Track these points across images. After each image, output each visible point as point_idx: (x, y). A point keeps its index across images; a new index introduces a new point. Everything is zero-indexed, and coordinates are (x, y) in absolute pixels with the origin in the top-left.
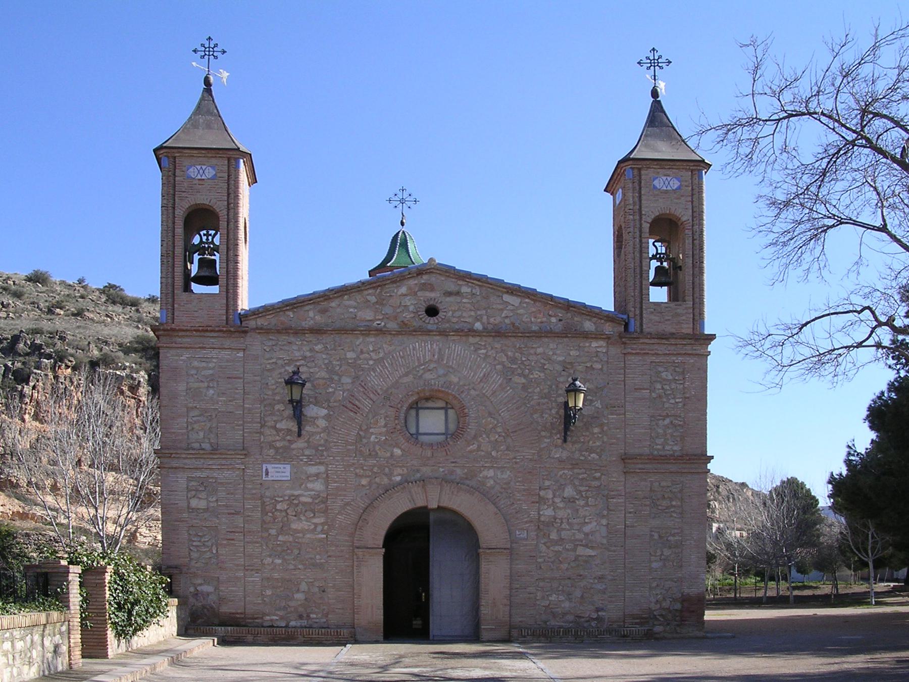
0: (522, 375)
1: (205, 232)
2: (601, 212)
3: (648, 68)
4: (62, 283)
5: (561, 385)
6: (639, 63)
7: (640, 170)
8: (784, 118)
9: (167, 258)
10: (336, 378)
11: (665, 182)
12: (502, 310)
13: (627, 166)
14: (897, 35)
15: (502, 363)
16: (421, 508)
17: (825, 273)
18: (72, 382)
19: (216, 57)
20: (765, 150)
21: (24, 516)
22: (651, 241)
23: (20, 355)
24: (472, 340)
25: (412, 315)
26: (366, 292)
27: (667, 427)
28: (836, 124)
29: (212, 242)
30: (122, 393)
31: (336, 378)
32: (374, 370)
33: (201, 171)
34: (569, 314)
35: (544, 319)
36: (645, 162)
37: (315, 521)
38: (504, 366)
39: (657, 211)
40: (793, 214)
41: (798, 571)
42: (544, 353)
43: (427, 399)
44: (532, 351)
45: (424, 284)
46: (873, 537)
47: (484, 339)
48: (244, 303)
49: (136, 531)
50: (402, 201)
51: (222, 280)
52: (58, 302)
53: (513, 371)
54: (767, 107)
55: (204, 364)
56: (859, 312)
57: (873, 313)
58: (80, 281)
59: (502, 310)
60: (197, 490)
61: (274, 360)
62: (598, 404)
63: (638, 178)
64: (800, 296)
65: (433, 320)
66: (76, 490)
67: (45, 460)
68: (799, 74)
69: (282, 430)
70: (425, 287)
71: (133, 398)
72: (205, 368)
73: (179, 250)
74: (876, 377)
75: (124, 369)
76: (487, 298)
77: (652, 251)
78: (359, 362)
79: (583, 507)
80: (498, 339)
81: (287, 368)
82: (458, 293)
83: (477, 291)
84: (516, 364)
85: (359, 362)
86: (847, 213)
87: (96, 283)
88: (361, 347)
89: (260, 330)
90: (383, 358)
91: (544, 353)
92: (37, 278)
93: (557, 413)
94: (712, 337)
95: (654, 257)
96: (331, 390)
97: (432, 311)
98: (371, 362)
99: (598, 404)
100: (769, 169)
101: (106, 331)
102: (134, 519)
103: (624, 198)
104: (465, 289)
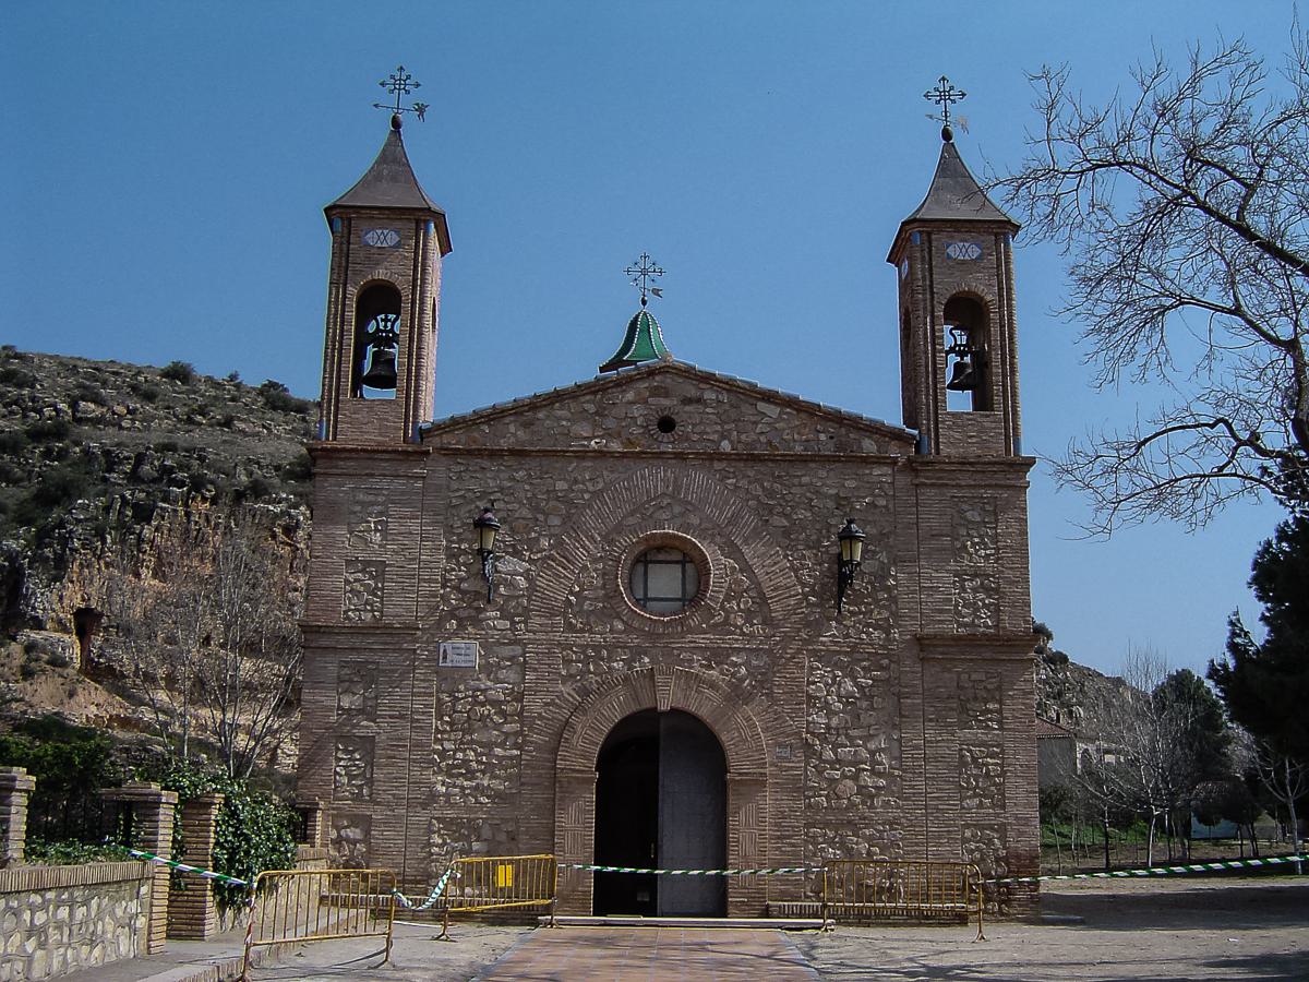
1: (383, 316)
4: (209, 379)
5: (833, 530)
7: (929, 234)
8: (1089, 169)
9: (334, 346)
11: (962, 250)
12: (756, 423)
14: (1221, 61)
15: (757, 498)
16: (647, 710)
17: (1167, 370)
18: (208, 521)
19: (408, 92)
20: (1069, 210)
21: (125, 723)
22: (947, 328)
23: (143, 482)
24: (717, 465)
25: (641, 431)
26: (582, 399)
27: (975, 590)
28: (1154, 178)
29: (392, 330)
30: (274, 536)
32: (590, 507)
34: (843, 429)
36: (932, 225)
39: (952, 285)
40: (1109, 293)
41: (1200, 821)
42: (811, 484)
43: (659, 549)
44: (796, 481)
45: (656, 388)
46: (1291, 765)
48: (428, 414)
50: (644, 272)
51: (402, 382)
52: (200, 406)
53: (771, 509)
54: (1066, 155)
55: (371, 498)
56: (1212, 426)
57: (1229, 426)
58: (233, 377)
59: (756, 423)
63: (927, 244)
64: (1134, 404)
65: (666, 437)
66: (200, 683)
67: (161, 636)
70: (656, 392)
71: (288, 544)
73: (351, 339)
74: (1263, 517)
75: (279, 502)
77: (948, 342)
80: (750, 464)
81: (478, 503)
82: (699, 400)
83: (725, 397)
86: (1189, 288)
87: (253, 379)
89: (449, 453)
90: (601, 491)
91: (811, 484)
92: (179, 373)
93: (829, 568)
94: (1030, 462)
95: (952, 350)
96: (533, 535)
97: (667, 425)
98: (586, 496)
100: (1075, 234)
102: (276, 726)
104: (709, 395)
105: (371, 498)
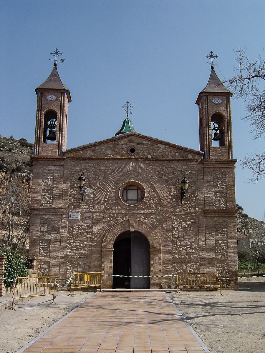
0: (166, 176)
1: (52, 120)
2: (193, 112)
3: (210, 58)
4: (5, 138)
6: (217, 56)
7: (207, 96)
8: (251, 78)
10: (97, 177)
11: (216, 101)
13: (203, 95)
15: (158, 171)
18: (4, 178)
19: (59, 56)
24: (147, 162)
25: (125, 152)
26: (109, 143)
29: (55, 124)
31: (97, 177)
32: (111, 174)
33: (51, 97)
35: (174, 154)
37: (88, 236)
38: (159, 172)
39: (214, 111)
43: (131, 186)
44: (169, 166)
47: (152, 161)
48: (65, 148)
49: (25, 241)
50: (127, 107)
51: (57, 139)
52: (2, 146)
53: (162, 174)
54: (245, 74)
55: (49, 172)
58: (11, 137)
59: (158, 150)
60: (44, 223)
61: (75, 170)
62: (194, 188)
65: (133, 154)
68: (255, 62)
69: (77, 198)
70: (130, 141)
72: (49, 173)
76: (153, 145)
78: (106, 171)
79: (189, 231)
81: (79, 173)
82: (142, 144)
84: (163, 172)
85: (106, 171)
87: (17, 138)
88: (106, 165)
89: (72, 159)
93: (179, 191)
94: (236, 161)
95: (214, 129)
96: (95, 182)
97: (133, 151)
99: (194, 188)
101: (19, 157)
103: (202, 107)
104: (145, 142)
105: (49, 172)
